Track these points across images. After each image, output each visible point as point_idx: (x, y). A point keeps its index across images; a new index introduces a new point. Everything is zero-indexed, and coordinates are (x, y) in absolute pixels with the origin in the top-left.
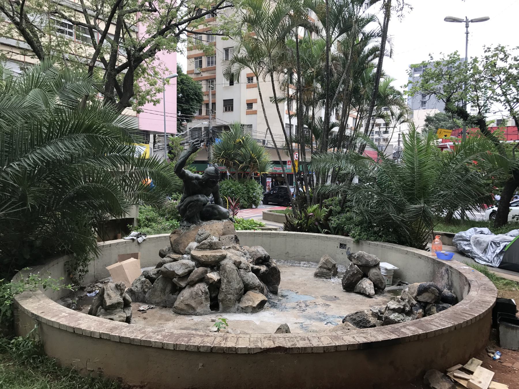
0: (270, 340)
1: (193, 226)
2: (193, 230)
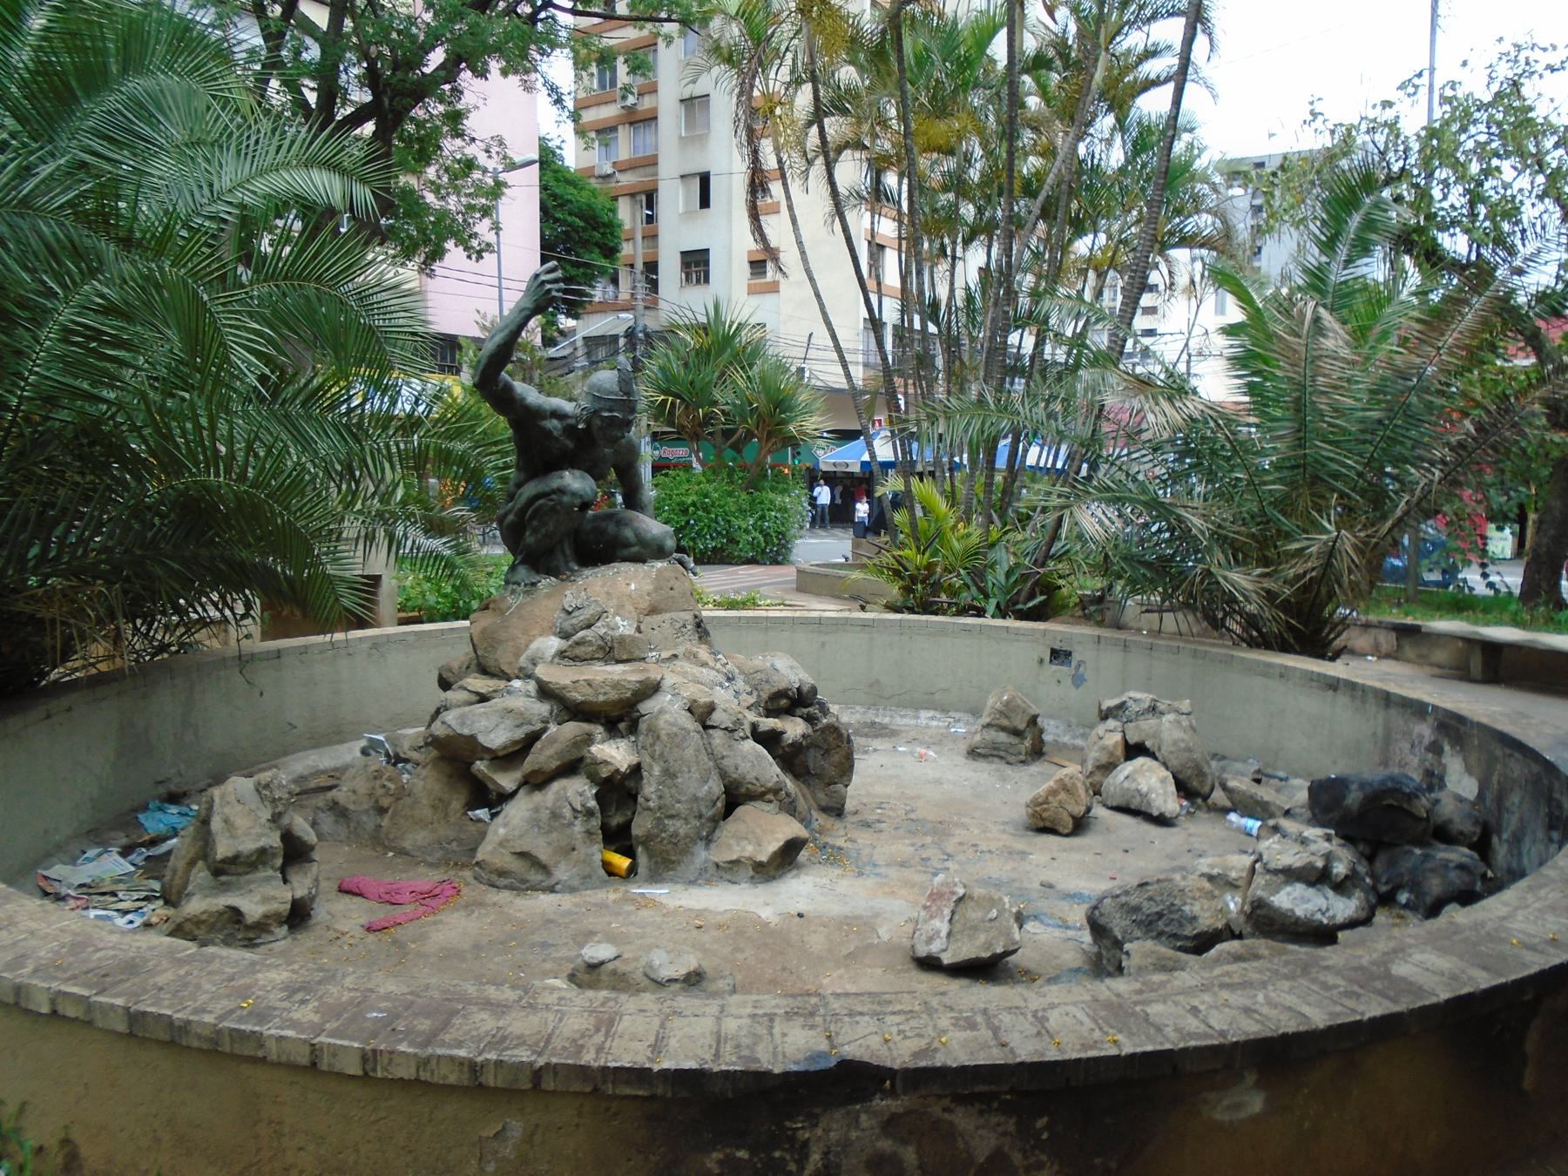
0: (812, 1027)
1: (546, 583)
2: (548, 596)
